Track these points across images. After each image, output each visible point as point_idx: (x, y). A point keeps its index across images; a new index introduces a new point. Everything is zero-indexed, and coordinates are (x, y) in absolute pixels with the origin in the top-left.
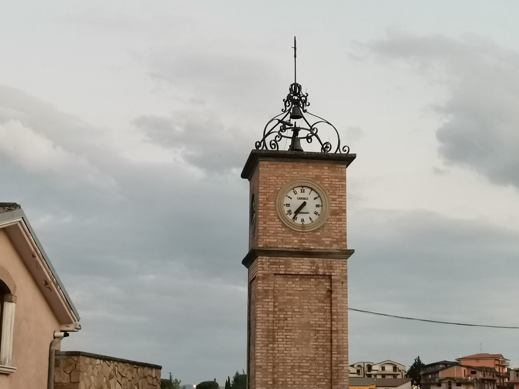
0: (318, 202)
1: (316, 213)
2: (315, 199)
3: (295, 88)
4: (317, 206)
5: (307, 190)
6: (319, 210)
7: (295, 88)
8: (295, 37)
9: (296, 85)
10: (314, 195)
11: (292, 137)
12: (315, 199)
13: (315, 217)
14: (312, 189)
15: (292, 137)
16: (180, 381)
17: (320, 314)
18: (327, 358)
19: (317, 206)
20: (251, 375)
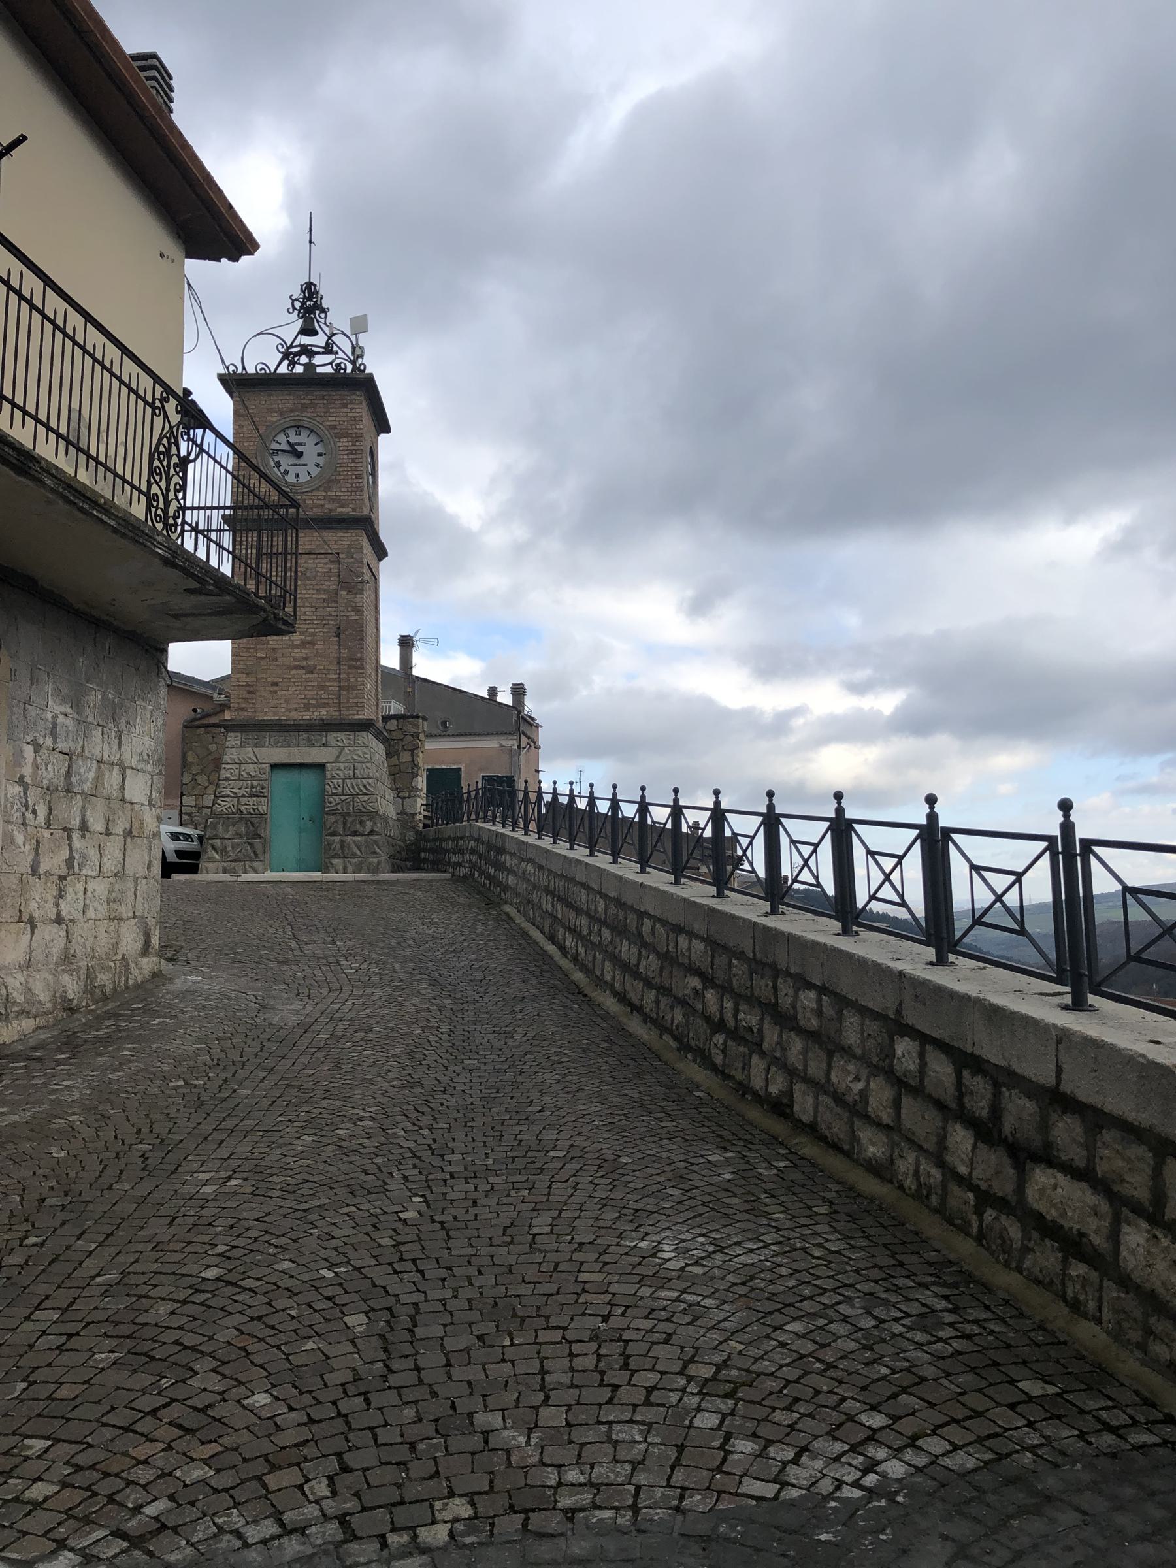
0: (320, 449)
1: (317, 465)
2: (316, 444)
3: (310, 290)
4: (320, 454)
5: (304, 433)
6: (321, 460)
7: (310, 290)
8: (22, 139)
9: (309, 284)
10: (314, 439)
11: (416, 672)
12: (316, 444)
13: (315, 471)
14: (312, 431)
15: (416, 672)
16: (518, 691)
17: (312, 630)
18: (472, 1504)
19: (320, 454)
20: (1147, 1394)
